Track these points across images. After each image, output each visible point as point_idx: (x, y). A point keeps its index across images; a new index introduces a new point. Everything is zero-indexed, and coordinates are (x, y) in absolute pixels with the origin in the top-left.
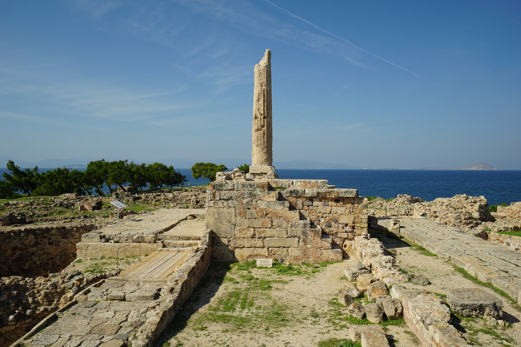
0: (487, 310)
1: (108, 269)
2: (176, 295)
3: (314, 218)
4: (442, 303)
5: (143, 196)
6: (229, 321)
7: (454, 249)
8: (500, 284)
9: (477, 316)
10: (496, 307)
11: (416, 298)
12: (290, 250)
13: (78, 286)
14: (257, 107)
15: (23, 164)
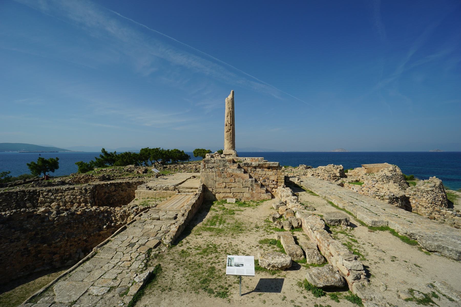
0: (343, 222)
1: (151, 204)
2: (186, 217)
3: (257, 177)
4: (321, 219)
5: (168, 166)
6: (213, 230)
7: (328, 192)
8: (349, 209)
9: (338, 225)
10: (347, 220)
11: (308, 218)
12: (244, 194)
13: (136, 212)
14: (227, 119)
15: (109, 150)
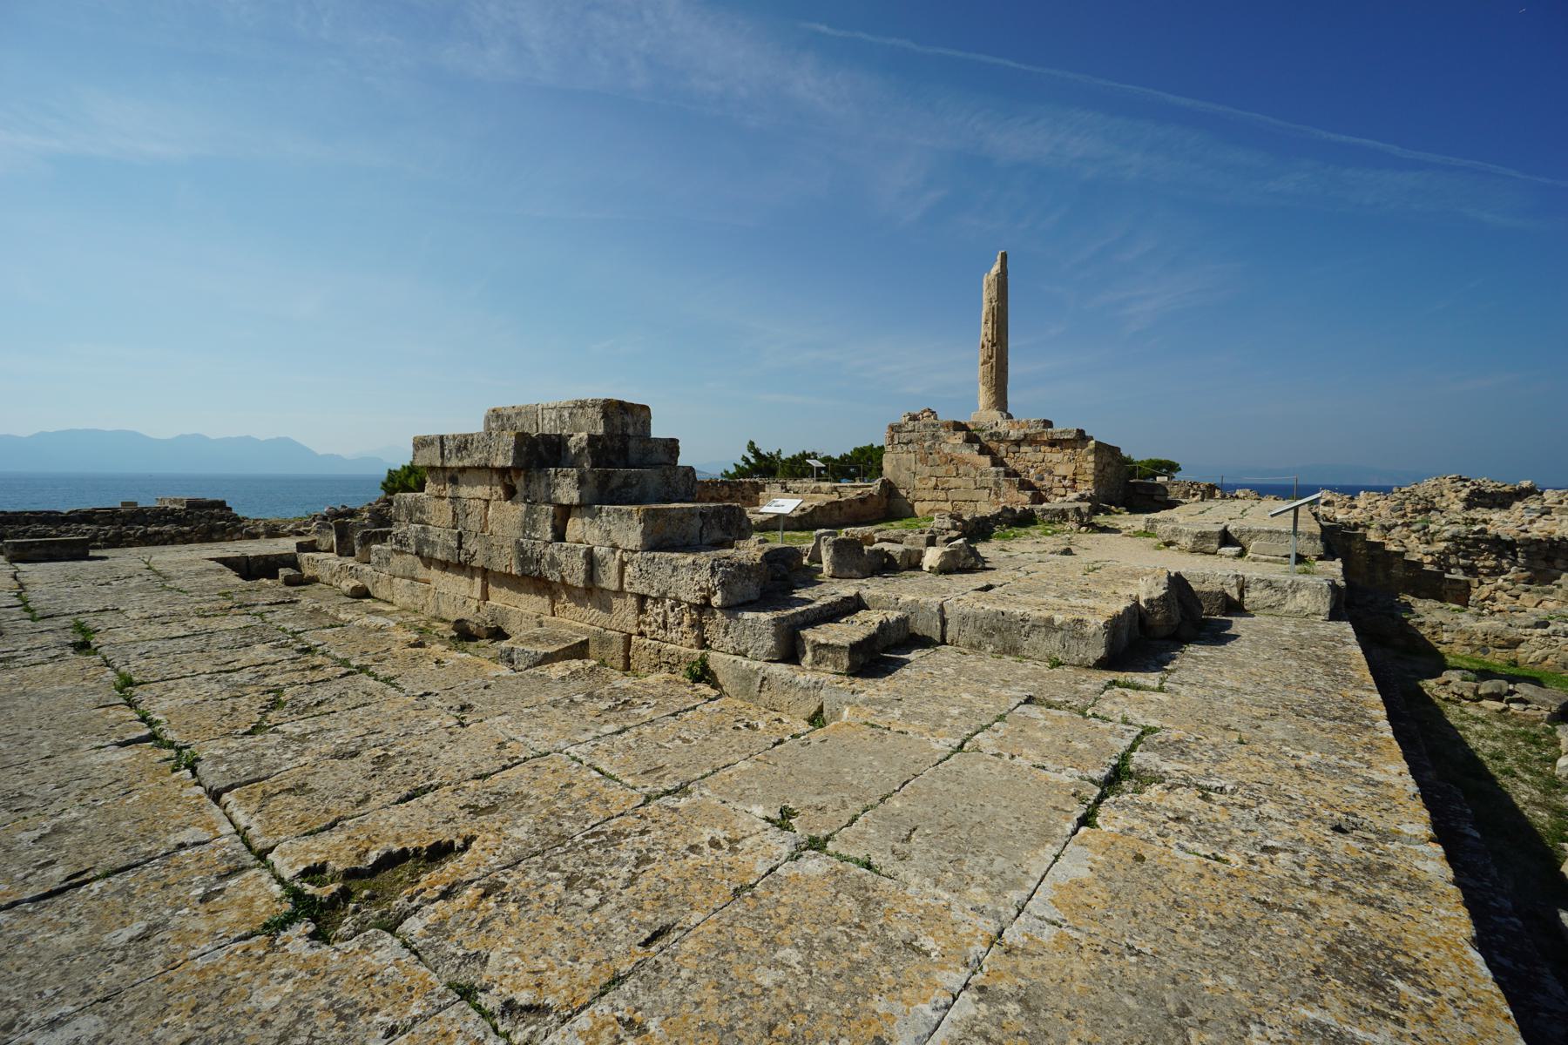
14: (985, 331)
